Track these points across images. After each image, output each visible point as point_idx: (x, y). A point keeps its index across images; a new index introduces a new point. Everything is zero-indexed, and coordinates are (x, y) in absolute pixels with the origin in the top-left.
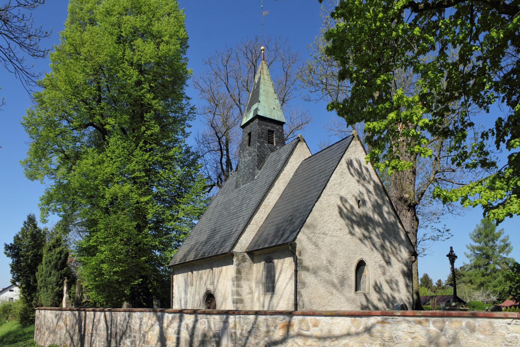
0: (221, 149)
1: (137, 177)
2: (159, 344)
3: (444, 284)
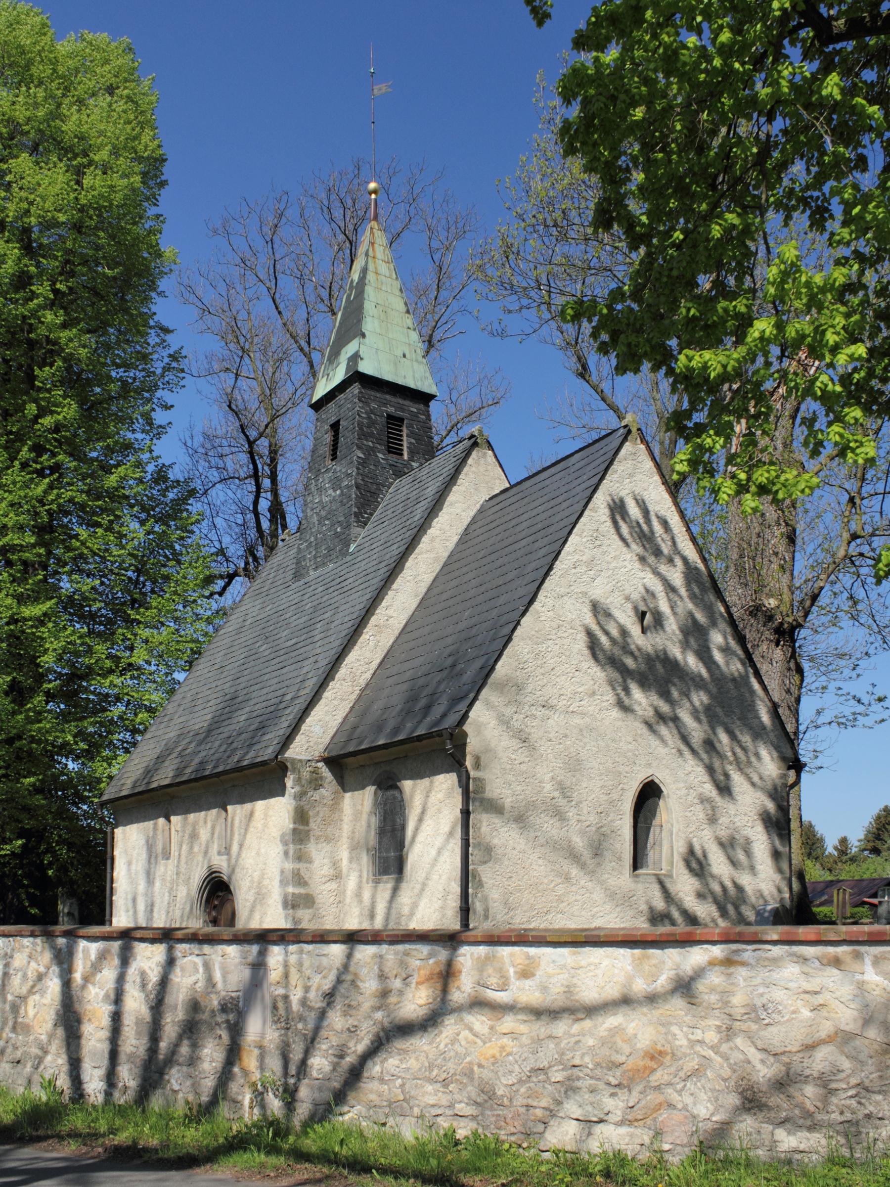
0: (256, 476)
1: (13, 548)
2: (60, 1032)
3: (854, 850)
